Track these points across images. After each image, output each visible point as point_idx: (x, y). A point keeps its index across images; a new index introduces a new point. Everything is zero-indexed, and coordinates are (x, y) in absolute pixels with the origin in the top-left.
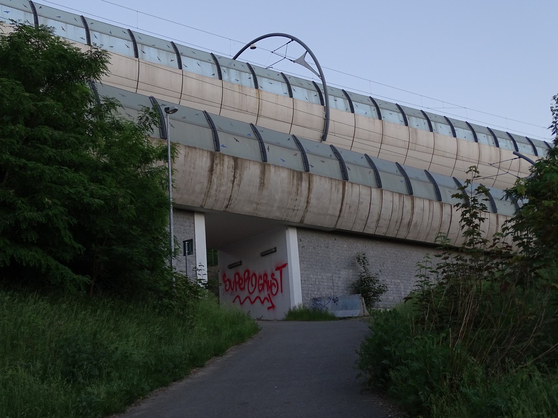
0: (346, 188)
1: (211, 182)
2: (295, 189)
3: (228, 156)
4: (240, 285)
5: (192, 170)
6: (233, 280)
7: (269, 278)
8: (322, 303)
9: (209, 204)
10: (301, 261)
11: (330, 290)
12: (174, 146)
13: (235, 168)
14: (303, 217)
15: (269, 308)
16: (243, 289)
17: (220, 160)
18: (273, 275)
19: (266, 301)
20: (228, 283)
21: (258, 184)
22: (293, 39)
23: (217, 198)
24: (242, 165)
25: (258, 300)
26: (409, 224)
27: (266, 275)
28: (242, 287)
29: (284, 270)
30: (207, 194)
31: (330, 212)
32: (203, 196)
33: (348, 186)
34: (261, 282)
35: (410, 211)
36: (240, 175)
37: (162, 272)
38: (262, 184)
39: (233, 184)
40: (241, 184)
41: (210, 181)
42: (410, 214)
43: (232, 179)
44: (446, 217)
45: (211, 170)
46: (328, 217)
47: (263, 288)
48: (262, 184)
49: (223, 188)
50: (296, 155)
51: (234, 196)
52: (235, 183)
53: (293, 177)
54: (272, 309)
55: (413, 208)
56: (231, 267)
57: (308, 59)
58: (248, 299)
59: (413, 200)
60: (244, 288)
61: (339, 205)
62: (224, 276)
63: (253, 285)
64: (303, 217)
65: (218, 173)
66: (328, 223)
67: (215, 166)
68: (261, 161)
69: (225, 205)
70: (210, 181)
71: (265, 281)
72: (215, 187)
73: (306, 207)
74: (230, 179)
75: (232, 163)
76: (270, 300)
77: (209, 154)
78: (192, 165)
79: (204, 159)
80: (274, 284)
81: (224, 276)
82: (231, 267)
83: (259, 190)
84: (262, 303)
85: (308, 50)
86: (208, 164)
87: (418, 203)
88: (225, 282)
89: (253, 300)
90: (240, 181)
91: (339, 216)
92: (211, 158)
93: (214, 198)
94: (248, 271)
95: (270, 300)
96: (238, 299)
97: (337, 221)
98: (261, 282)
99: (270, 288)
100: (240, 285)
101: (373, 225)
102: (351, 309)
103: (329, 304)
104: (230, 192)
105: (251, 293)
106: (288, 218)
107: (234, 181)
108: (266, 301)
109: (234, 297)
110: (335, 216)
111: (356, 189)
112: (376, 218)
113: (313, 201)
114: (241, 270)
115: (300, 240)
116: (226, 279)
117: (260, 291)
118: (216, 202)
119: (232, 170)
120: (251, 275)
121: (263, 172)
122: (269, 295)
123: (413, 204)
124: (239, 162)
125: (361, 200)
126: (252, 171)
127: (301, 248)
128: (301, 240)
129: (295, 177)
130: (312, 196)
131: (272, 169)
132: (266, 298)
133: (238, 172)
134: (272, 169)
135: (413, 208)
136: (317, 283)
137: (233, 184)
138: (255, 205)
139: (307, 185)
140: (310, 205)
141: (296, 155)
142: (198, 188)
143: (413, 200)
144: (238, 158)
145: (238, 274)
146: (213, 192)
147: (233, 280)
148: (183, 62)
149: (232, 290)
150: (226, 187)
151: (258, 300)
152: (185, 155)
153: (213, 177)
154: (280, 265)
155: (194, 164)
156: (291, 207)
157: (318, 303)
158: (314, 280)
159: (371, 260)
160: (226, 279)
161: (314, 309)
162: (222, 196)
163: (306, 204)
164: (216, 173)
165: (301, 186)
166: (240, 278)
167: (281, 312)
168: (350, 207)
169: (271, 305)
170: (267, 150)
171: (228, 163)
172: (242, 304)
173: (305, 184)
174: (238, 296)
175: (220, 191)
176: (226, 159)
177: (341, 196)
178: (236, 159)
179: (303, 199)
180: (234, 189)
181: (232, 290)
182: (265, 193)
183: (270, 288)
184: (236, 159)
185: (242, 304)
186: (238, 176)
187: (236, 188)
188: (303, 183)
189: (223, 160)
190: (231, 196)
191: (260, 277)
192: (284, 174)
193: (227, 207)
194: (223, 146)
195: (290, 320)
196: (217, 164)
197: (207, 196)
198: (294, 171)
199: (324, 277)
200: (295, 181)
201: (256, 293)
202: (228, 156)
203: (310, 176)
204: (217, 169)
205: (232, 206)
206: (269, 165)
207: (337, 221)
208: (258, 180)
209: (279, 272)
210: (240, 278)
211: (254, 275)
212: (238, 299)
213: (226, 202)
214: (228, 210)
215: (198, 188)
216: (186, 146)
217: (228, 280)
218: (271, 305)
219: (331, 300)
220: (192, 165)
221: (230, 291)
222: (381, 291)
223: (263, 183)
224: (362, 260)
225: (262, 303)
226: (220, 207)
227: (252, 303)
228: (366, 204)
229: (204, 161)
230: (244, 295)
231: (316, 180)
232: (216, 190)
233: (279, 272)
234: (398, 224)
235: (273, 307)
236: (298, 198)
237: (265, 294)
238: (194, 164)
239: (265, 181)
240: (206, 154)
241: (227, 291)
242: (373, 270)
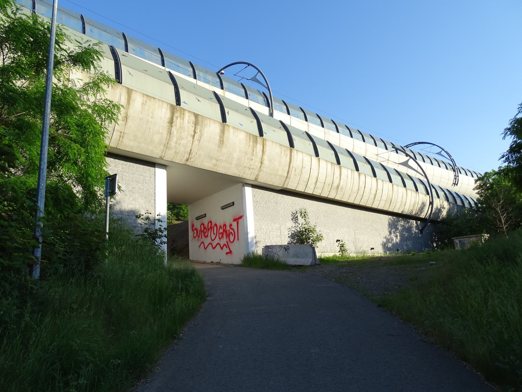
0: (293, 154)
1: (170, 133)
2: (250, 150)
3: (189, 111)
4: (204, 233)
5: (150, 119)
6: (199, 229)
7: (228, 228)
8: (274, 250)
9: (169, 156)
10: (255, 214)
11: (278, 239)
12: (118, 80)
13: (196, 124)
14: (258, 175)
15: (227, 253)
16: (206, 237)
17: (181, 114)
18: (231, 225)
19: (225, 247)
20: (195, 231)
21: (218, 142)
22: (249, 64)
23: (177, 151)
24: (202, 122)
25: (218, 246)
26: (338, 187)
27: (225, 225)
28: (206, 235)
29: (240, 221)
30: (167, 146)
31: (280, 173)
32: (162, 147)
33: (294, 152)
34: (221, 231)
35: (339, 177)
36: (200, 131)
37: (482, 236)
38: (222, 142)
39: (193, 138)
40: (202, 140)
41: (170, 133)
42: (338, 179)
43: (193, 133)
44: (362, 184)
45: (171, 122)
46: (278, 177)
47: (222, 236)
48: (222, 142)
49: (183, 142)
50: (252, 122)
51: (195, 150)
52: (195, 138)
53: (250, 139)
54: (229, 254)
55: (341, 174)
56: (198, 218)
57: (259, 77)
58: (210, 245)
59: (340, 168)
60: (208, 235)
61: (287, 168)
62: (193, 226)
63: (214, 234)
64: (258, 175)
65: (178, 126)
66: (278, 183)
67: (175, 118)
68: (221, 121)
69: (185, 158)
70: (170, 133)
71: (224, 230)
72: (175, 139)
73: (260, 167)
74: (190, 133)
75: (193, 118)
76: (227, 246)
77: (169, 107)
78: (151, 115)
79: (164, 110)
80: (231, 233)
81: (193, 226)
82: (198, 218)
83: (219, 147)
84: (222, 248)
85: (259, 71)
86: (168, 115)
87: (344, 170)
88: (193, 231)
89: (214, 246)
90: (201, 137)
91: (287, 177)
92: (171, 111)
93: (174, 150)
94: (211, 222)
95: (227, 246)
96: (202, 245)
97: (285, 181)
98: (221, 231)
99: (228, 236)
100: (204, 233)
101: (312, 186)
102: (303, 258)
103: (281, 252)
104: (191, 145)
105: (212, 240)
106: (245, 176)
107: (194, 136)
108: (225, 247)
109: (200, 243)
110: (283, 177)
111: (300, 155)
112: (315, 180)
113: (266, 162)
114: (205, 221)
115: (254, 196)
116: (194, 228)
117: (220, 239)
118: (176, 154)
119: (192, 124)
120: (213, 225)
121: (223, 132)
122: (227, 242)
123: (341, 171)
124: (200, 119)
125: (304, 165)
126: (213, 128)
127: (255, 202)
128: (255, 196)
129: (252, 140)
130: (265, 157)
131: (231, 130)
132: (224, 245)
133: (199, 127)
134: (231, 130)
135: (341, 174)
136: (268, 232)
137: (193, 138)
138: (214, 161)
139: (262, 148)
140: (263, 165)
141: (252, 122)
142: (156, 138)
143: (340, 168)
144: (198, 115)
145: (203, 224)
146: (173, 144)
147: (199, 229)
148: (182, 99)
149: (199, 237)
150: (186, 141)
151: (218, 246)
152: (143, 103)
153: (173, 129)
154: (237, 217)
155: (152, 113)
156: (248, 166)
157: (270, 250)
158: (265, 229)
159: (310, 215)
160: (194, 228)
161: (267, 256)
162: (182, 149)
163: (260, 164)
164: (176, 126)
165: (256, 148)
166: (205, 228)
167: (237, 258)
168: (295, 170)
169: (229, 251)
170: (227, 114)
171: (189, 118)
172: (205, 249)
173: (259, 147)
174: (203, 242)
175: (180, 144)
176: (187, 114)
177: (289, 160)
178: (196, 116)
179: (258, 160)
180: (194, 144)
181: (199, 237)
182: (224, 150)
183: (228, 236)
184: (196, 116)
185: (205, 249)
186: (198, 131)
187: (196, 142)
188: (258, 146)
189: (184, 114)
190: (191, 150)
191: (221, 227)
192: (242, 136)
193: (187, 160)
194: (184, 103)
195: (245, 266)
196: (177, 117)
197: (167, 148)
198: (250, 134)
199: (274, 228)
200: (251, 143)
201: (217, 241)
202: (189, 111)
203: (264, 141)
204: (178, 122)
205: (192, 160)
206: (228, 126)
207: (285, 181)
208: (218, 138)
209: (236, 222)
210: (205, 228)
211: (216, 225)
212: (202, 245)
213: (187, 156)
214: (188, 163)
215: (156, 138)
216: (144, 94)
217: (196, 229)
218: (229, 251)
219: (283, 249)
220: (151, 115)
221: (197, 238)
222: (319, 239)
223: (223, 141)
224: (304, 215)
225: (222, 248)
226: (180, 159)
227: (214, 248)
228: (306, 170)
229: (164, 113)
230: (207, 241)
231: (268, 144)
232: (176, 143)
233: (236, 222)
234: (330, 186)
235: (231, 252)
236: (254, 158)
237: (223, 241)
238: (152, 113)
239: (224, 139)
240: (165, 105)
241: (194, 237)
242: (312, 222)
